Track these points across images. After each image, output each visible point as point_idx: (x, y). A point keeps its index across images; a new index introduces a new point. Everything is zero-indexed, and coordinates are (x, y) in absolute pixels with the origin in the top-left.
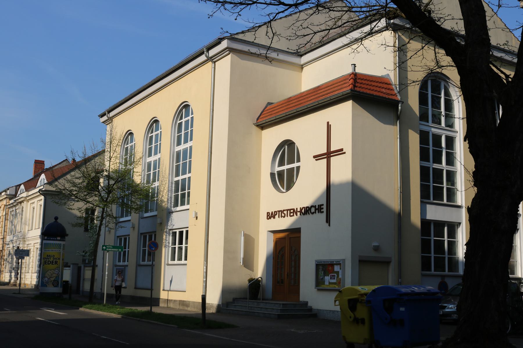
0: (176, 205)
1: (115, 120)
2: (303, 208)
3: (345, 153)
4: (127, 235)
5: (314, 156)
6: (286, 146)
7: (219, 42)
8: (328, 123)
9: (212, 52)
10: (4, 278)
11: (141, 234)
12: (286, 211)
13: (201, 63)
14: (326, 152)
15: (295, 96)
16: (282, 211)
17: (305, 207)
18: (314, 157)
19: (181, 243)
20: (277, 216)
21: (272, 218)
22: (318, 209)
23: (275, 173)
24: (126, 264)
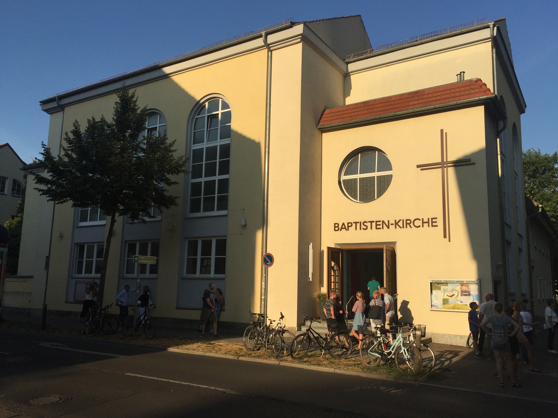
1: (67, 110)
2: (400, 220)
5: (417, 166)
6: (360, 154)
8: (442, 131)
9: (271, 38)
11: (126, 241)
13: (256, 48)
14: (440, 161)
18: (418, 166)
20: (352, 229)
23: (341, 182)
24: (93, 276)
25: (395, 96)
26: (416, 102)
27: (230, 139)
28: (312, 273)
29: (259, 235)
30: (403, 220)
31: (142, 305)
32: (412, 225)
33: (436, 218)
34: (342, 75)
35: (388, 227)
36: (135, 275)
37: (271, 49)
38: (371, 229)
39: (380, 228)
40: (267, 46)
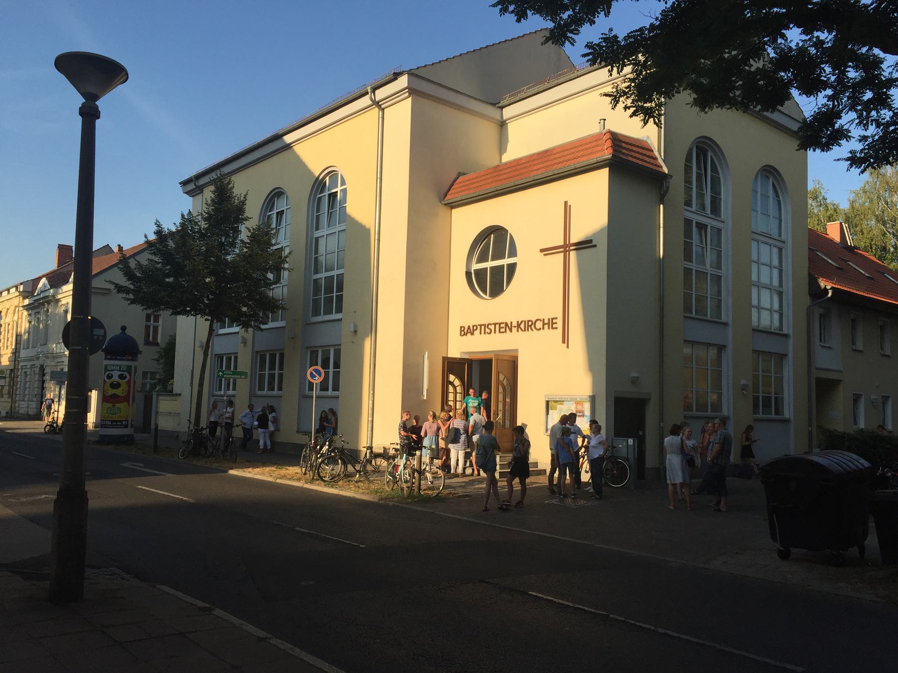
0: (316, 313)
2: (522, 321)
3: (595, 246)
4: (319, 347)
6: (492, 235)
7: (396, 76)
8: (566, 203)
9: (381, 94)
10: (17, 408)
11: (257, 352)
12: (493, 326)
15: (506, 164)
16: (486, 326)
17: (525, 321)
18: (542, 251)
19: (272, 367)
20: (477, 332)
21: (469, 334)
22: (548, 324)
23: (471, 273)
25: (526, 157)
26: (541, 166)
27: (345, 224)
28: (427, 390)
29: (368, 344)
30: (525, 321)
31: (260, 426)
32: (533, 327)
33: (556, 318)
34: (497, 124)
35: (511, 330)
36: (222, 392)
37: (382, 106)
38: (495, 332)
39: (503, 332)
40: (377, 104)
